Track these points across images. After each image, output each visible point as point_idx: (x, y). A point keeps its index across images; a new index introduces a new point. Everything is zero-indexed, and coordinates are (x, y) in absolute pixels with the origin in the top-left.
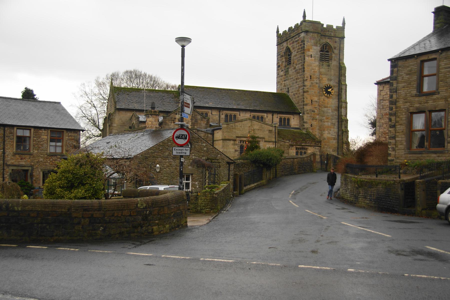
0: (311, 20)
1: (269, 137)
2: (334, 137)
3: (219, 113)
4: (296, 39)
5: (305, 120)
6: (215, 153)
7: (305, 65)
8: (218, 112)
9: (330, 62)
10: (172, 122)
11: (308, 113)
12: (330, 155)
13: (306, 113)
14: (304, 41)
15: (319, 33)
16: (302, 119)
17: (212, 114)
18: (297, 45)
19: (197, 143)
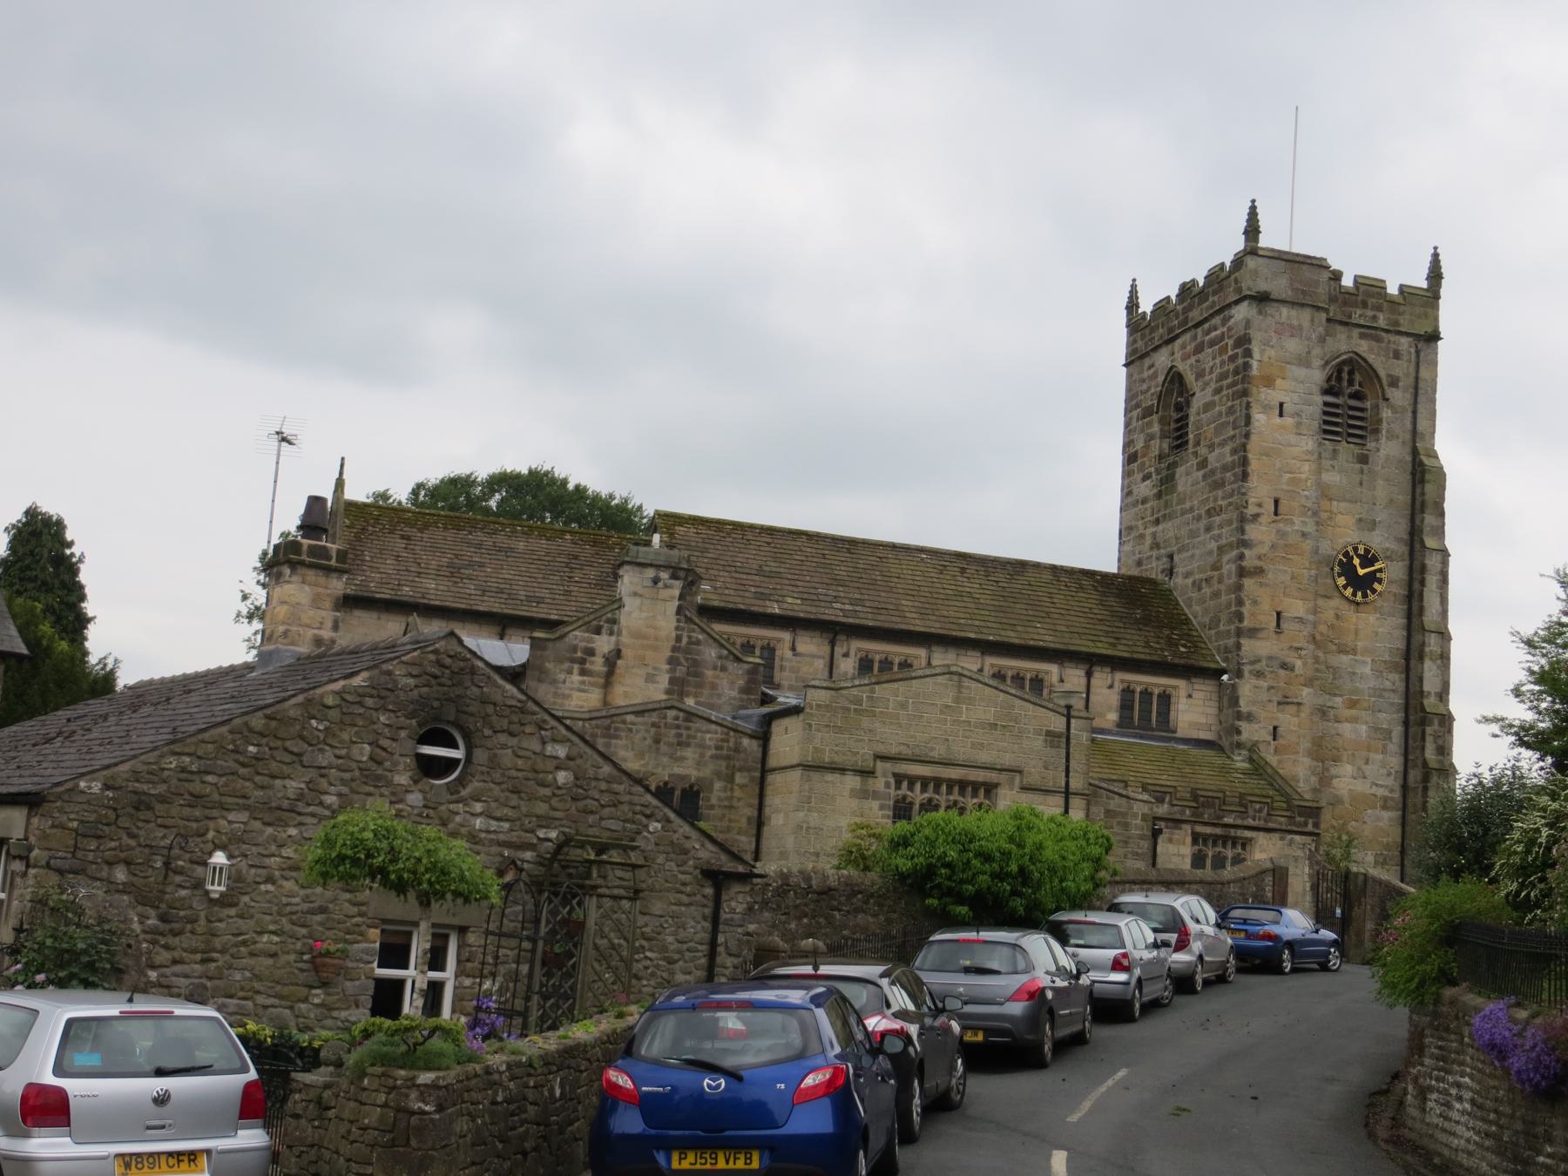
0: (1286, 248)
2: (1387, 793)
3: (826, 649)
4: (1213, 334)
5: (1244, 706)
6: (625, 808)
7: (1248, 447)
8: (826, 642)
9: (1371, 445)
10: (576, 666)
11: (1259, 674)
12: (1361, 878)
14: (1249, 341)
15: (1318, 308)
16: (1228, 699)
17: (793, 649)
18: (1218, 361)
19: (512, 734)
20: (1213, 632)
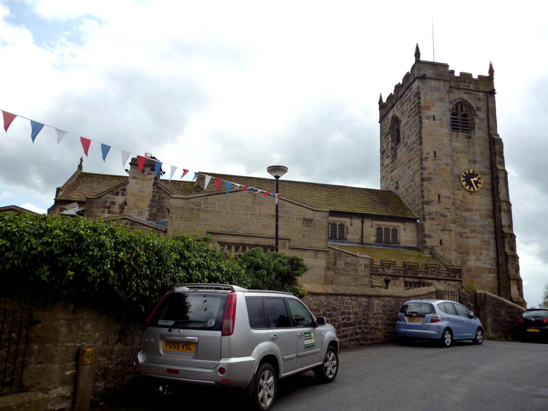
1: (304, 237)
2: (490, 267)
5: (427, 232)
7: (422, 132)
10: (106, 210)
11: (432, 219)
12: (483, 296)
13: (429, 218)
16: (420, 229)
18: (409, 106)
20: (413, 205)
